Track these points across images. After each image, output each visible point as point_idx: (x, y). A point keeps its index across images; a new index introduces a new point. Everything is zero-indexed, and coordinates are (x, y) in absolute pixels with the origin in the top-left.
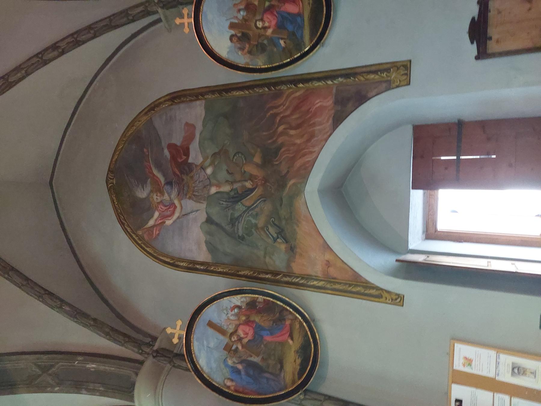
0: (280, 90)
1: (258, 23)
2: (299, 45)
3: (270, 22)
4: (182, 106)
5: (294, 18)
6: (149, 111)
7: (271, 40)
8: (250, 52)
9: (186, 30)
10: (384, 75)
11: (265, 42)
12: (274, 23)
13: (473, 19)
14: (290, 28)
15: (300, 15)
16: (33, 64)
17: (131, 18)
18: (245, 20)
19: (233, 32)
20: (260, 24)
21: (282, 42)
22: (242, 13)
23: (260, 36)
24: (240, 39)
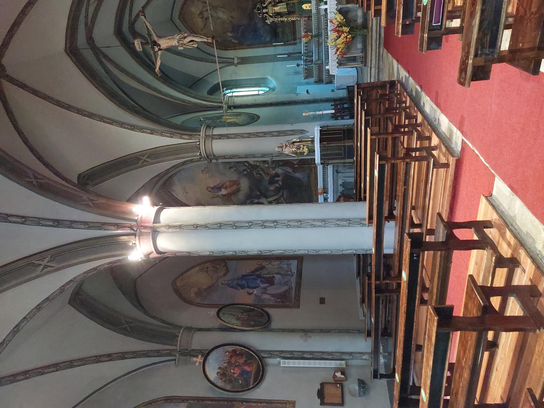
0: (233, 404)
1: (231, 370)
2: (248, 384)
3: (237, 371)
4: (172, 404)
5: (248, 373)
6: (148, 404)
7: (235, 378)
8: (224, 381)
9: (197, 364)
10: (284, 405)
11: (233, 379)
12: (239, 372)
13: (319, 389)
14: (245, 376)
15: (251, 372)
16: (92, 360)
17: (160, 354)
18: (226, 367)
19: (219, 371)
20: (232, 371)
21: (240, 381)
22: (225, 364)
23: (231, 376)
24: (222, 375)
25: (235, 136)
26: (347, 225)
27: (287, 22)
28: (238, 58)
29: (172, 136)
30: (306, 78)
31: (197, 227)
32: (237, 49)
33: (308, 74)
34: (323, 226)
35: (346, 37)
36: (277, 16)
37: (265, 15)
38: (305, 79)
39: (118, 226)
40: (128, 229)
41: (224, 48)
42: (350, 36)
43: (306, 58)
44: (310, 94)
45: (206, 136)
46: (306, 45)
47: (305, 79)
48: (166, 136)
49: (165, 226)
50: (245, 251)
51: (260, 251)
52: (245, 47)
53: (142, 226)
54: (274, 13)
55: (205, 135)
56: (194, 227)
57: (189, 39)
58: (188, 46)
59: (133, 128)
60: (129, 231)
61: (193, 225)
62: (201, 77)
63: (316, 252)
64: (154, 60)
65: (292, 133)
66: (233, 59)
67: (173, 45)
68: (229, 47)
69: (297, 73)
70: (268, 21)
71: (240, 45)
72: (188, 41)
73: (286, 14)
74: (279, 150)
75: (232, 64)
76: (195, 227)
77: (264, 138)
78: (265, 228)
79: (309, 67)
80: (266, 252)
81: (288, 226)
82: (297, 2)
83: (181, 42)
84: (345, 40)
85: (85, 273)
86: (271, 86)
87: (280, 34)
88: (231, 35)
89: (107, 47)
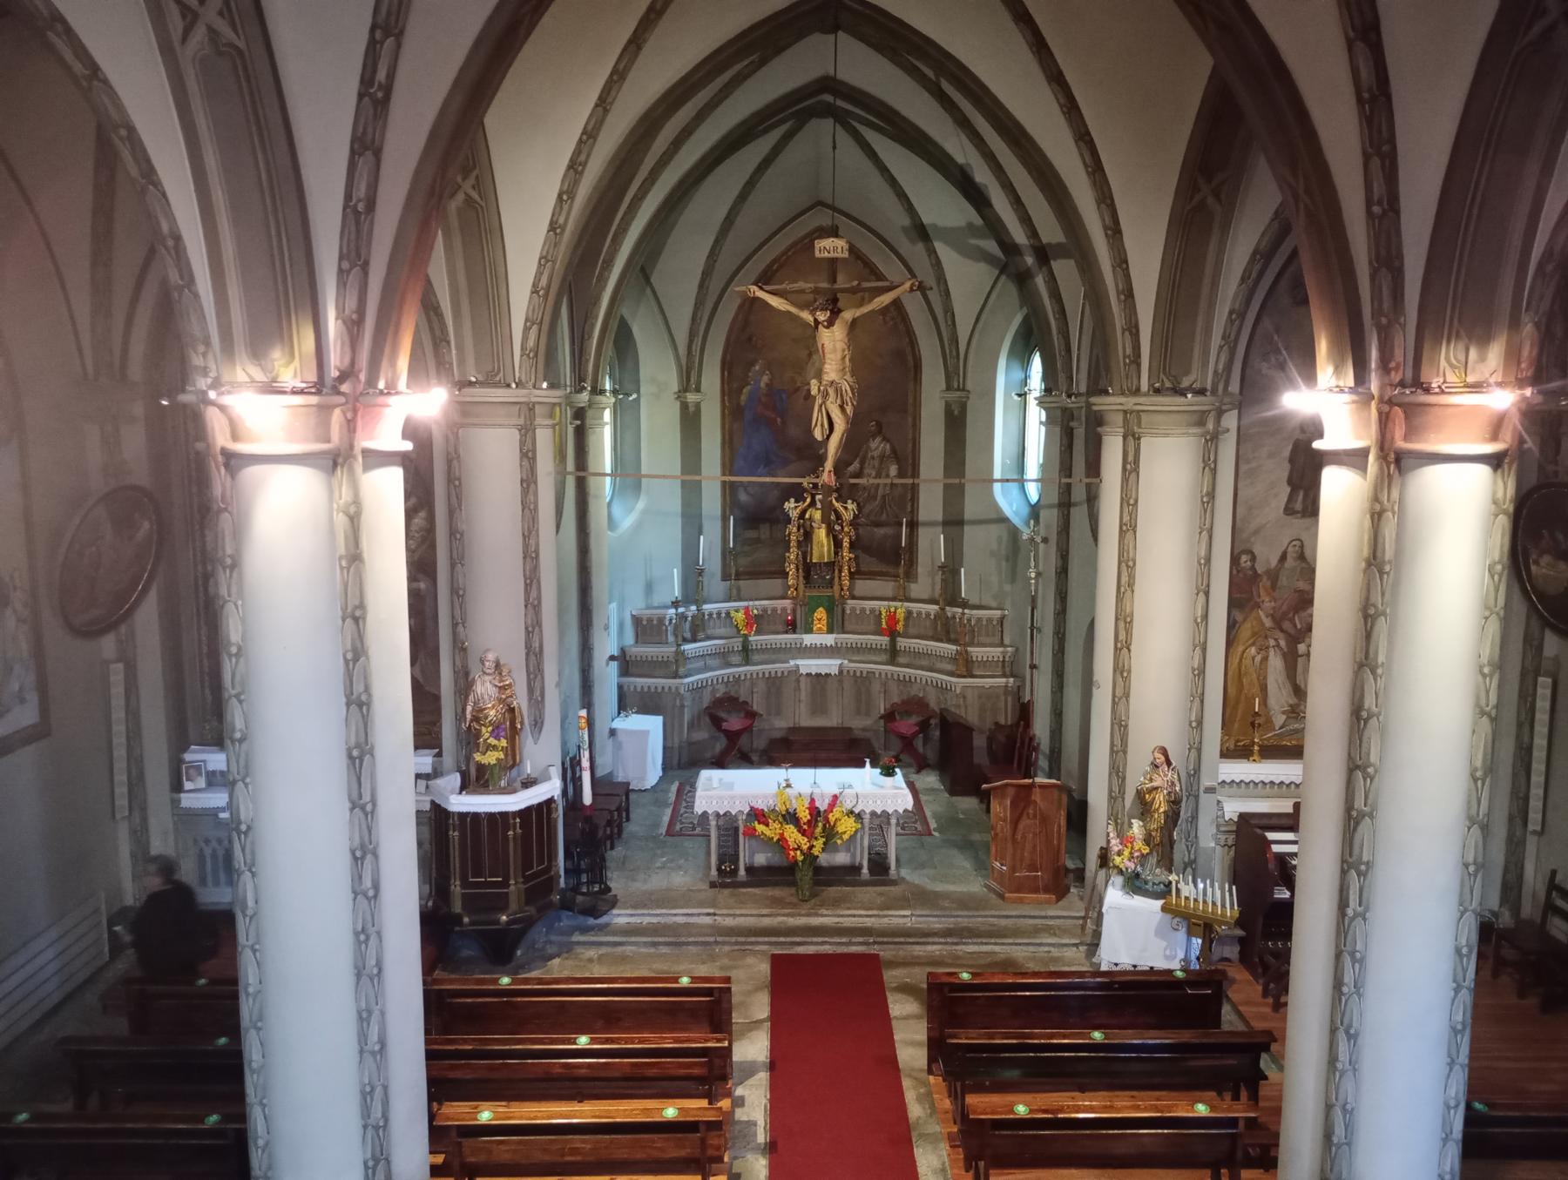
25: (532, 507)
26: (371, 1121)
27: (784, 559)
28: (698, 405)
29: (537, 292)
30: (637, 621)
31: (356, 620)
32: (723, 401)
33: (646, 628)
34: (366, 1048)
35: (799, 848)
36: (802, 531)
37: (808, 500)
38: (633, 616)
39: (353, 326)
40: (347, 361)
41: (728, 357)
42: (800, 858)
43: (690, 619)
44: (608, 664)
45: (531, 408)
46: (723, 615)
47: (633, 616)
48: (539, 274)
49: (357, 501)
50: (247, 775)
51: (249, 828)
52: (727, 426)
53: (355, 411)
54: (811, 526)
55: (534, 404)
56: (356, 607)
57: (839, 421)
58: (820, 410)
59: (576, 167)
60: (336, 359)
61: (362, 606)
62: (652, 280)
63: (254, 1018)
64: (783, 286)
65: (538, 693)
66: (698, 390)
67: (826, 366)
68: (729, 373)
69: (649, 588)
70: (792, 505)
71: (733, 412)
72: (833, 416)
73: (805, 558)
74: (487, 664)
75: (684, 388)
76: (358, 613)
77: (523, 603)
78: (355, 859)
79: (667, 630)
80: (248, 851)
81: (362, 937)
82: (833, 596)
83: (831, 391)
84: (792, 845)
85: (131, 130)
86: (617, 511)
87: (752, 534)
88: (762, 385)
89: (834, 142)
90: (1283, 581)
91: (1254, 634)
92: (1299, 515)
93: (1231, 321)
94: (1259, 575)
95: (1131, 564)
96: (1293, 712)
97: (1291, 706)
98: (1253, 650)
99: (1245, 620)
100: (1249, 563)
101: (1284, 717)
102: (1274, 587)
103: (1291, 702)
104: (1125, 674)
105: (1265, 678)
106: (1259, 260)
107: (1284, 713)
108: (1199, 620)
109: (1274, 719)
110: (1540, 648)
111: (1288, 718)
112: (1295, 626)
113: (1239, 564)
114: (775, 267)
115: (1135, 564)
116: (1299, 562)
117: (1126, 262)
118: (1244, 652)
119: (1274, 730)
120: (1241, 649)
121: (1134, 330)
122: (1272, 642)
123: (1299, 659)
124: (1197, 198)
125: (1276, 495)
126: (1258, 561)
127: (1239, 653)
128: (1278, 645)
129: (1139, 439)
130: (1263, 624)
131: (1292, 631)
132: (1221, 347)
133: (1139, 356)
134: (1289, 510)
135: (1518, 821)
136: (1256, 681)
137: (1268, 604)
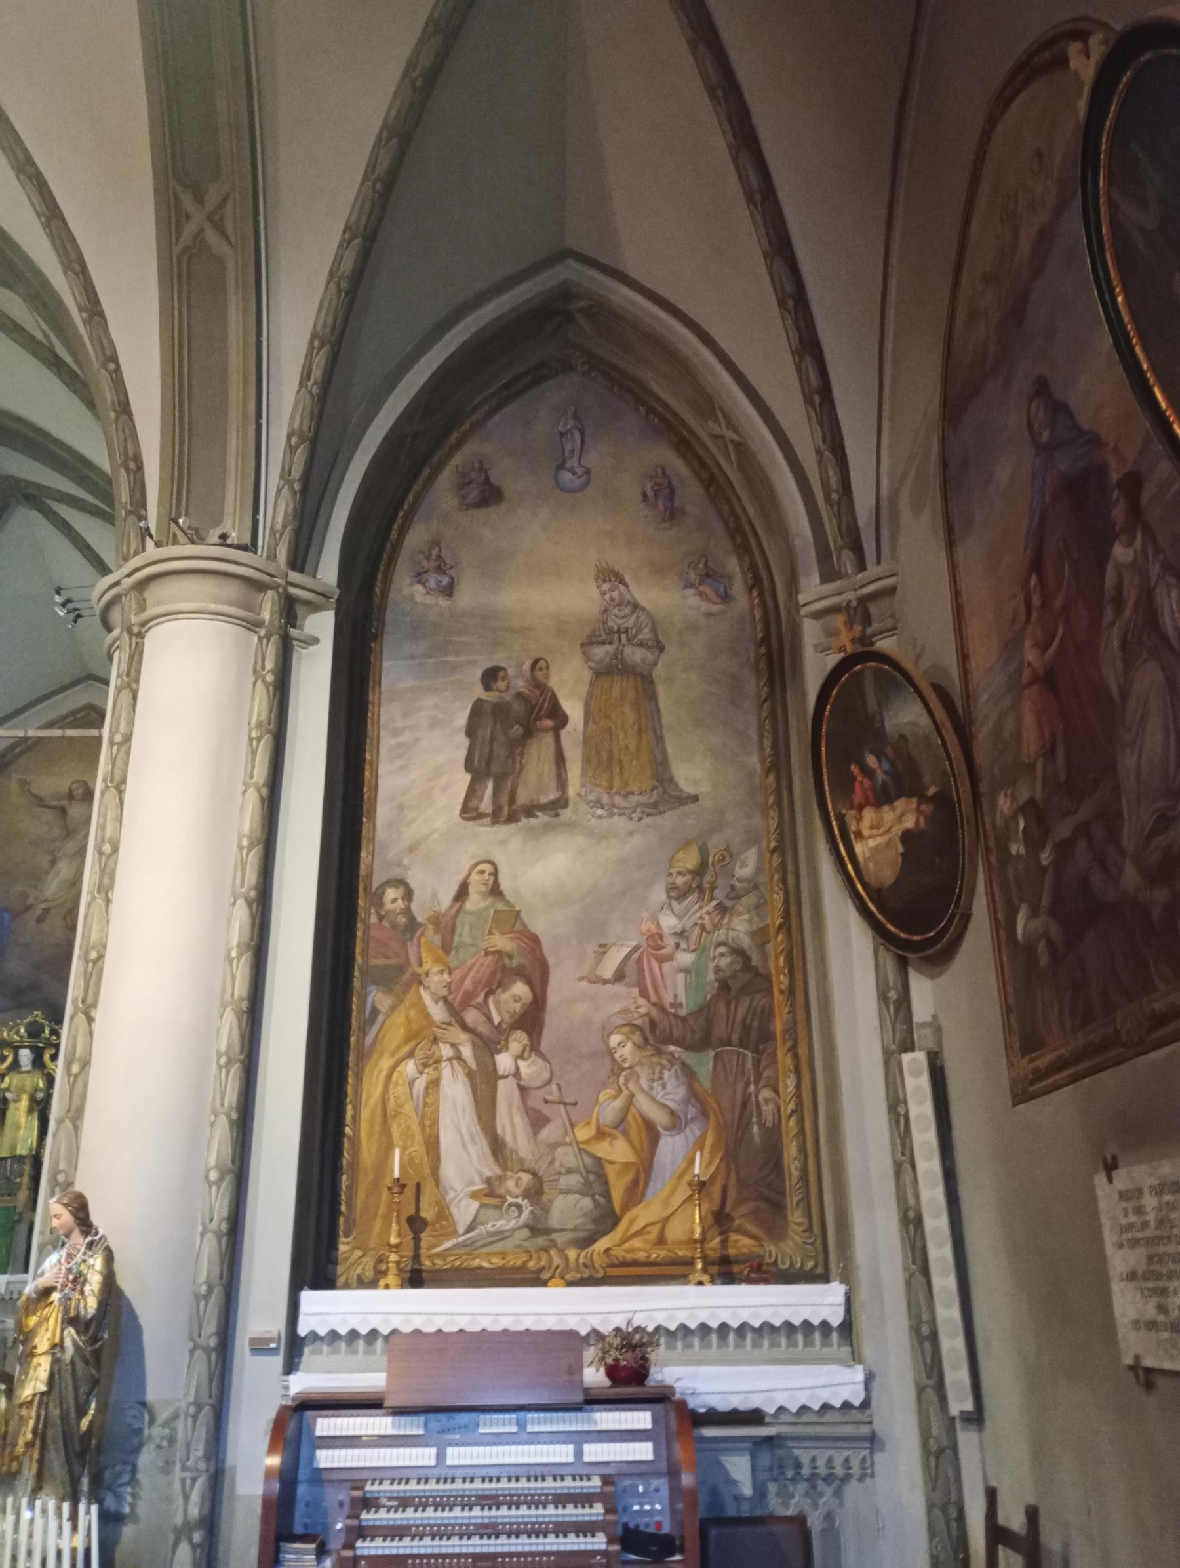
90: (464, 934)
91: (412, 1036)
92: (487, 820)
93: (291, 446)
94: (420, 925)
95: (107, 848)
96: (491, 1194)
97: (488, 1181)
98: (410, 1067)
99: (393, 1009)
100: (400, 902)
101: (475, 1205)
102: (447, 947)
103: (488, 1173)
104: (75, 1069)
105: (435, 1123)
106: (320, 349)
107: (474, 1195)
108: (234, 954)
109: (454, 1211)
110: (904, 1002)
111: (482, 1206)
112: (489, 1019)
113: (382, 905)
114: (17, 751)
115: (115, 850)
116: (490, 900)
117: (115, 360)
118: (393, 1069)
119: (455, 1233)
120: (385, 1063)
121: (132, 465)
122: (446, 1051)
123: (501, 1083)
124: (190, 229)
125: (445, 789)
126: (415, 897)
127: (384, 1074)
128: (458, 1057)
129: (141, 635)
130: (427, 1015)
131: (483, 1029)
132: (279, 491)
133: (143, 505)
134: (469, 811)
135: (931, 1395)
136: (415, 1127)
137: (437, 979)
